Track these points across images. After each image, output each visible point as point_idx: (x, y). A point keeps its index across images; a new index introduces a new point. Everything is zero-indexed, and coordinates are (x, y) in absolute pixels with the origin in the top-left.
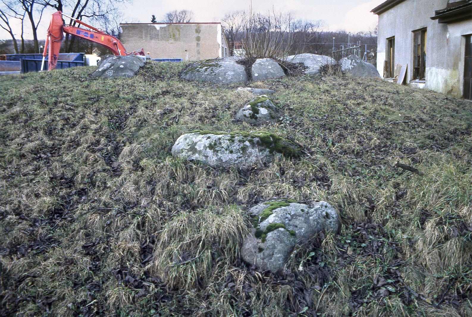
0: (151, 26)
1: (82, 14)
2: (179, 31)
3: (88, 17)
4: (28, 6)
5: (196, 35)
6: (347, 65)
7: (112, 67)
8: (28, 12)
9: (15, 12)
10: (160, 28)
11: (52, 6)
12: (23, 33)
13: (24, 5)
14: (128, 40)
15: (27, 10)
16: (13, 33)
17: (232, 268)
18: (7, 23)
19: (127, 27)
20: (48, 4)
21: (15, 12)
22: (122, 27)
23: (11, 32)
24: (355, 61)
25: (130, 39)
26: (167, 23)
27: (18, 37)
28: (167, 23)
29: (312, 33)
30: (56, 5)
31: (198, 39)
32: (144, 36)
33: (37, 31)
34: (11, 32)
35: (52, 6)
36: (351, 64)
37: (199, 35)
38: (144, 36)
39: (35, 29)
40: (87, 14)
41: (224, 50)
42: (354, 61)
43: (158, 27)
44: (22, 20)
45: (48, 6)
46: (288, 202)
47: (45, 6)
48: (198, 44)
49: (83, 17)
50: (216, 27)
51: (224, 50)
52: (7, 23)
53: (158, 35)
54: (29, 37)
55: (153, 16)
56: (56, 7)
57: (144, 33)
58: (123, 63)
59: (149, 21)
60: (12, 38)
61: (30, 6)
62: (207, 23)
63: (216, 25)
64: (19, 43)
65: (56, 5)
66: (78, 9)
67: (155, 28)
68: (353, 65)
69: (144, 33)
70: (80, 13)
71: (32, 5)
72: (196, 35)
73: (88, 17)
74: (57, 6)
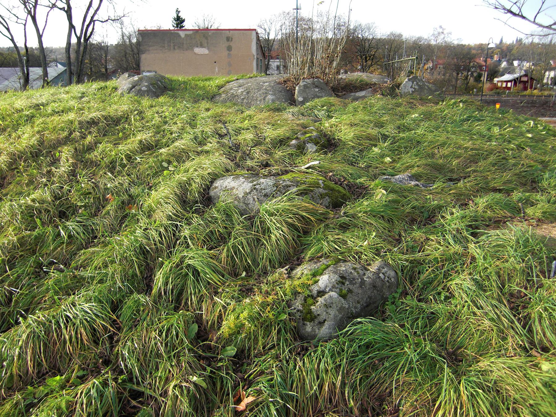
2: (207, 38)
3: (102, 22)
4: (31, 9)
5: (227, 44)
6: (407, 88)
8: (31, 15)
9: (17, 17)
10: (186, 35)
11: (61, 9)
12: (27, 42)
13: (26, 7)
14: (149, 50)
15: (29, 12)
16: (15, 41)
18: (8, 29)
19: (144, 34)
20: (54, 6)
21: (17, 17)
23: (12, 40)
24: (417, 84)
25: (151, 48)
27: (20, 44)
29: (265, 40)
30: (64, 8)
31: (229, 48)
32: (166, 45)
33: (43, 39)
34: (12, 40)
35: (61, 9)
36: (411, 87)
37: (231, 44)
38: (166, 45)
39: (40, 37)
41: (259, 60)
42: (415, 82)
44: (25, 25)
45: (55, 9)
46: (188, 310)
47: (52, 8)
48: (229, 54)
49: (96, 22)
50: (251, 34)
51: (259, 60)
52: (8, 29)
53: (183, 43)
54: (33, 43)
56: (64, 10)
57: (166, 42)
59: (168, 25)
60: (12, 45)
61: (33, 8)
63: (250, 32)
64: (23, 52)
65: (64, 8)
66: (89, 12)
67: (179, 36)
69: (166, 42)
70: (92, 17)
71: (35, 7)
72: (227, 44)
73: (102, 22)
74: (66, 9)
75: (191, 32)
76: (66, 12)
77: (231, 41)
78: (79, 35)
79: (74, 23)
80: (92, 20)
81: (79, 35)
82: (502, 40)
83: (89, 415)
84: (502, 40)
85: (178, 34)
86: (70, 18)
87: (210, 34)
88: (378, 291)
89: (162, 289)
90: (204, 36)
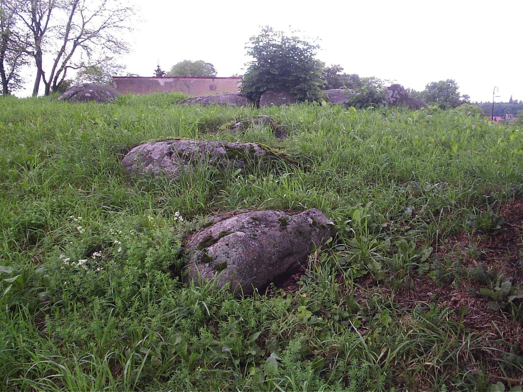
0: (153, 81)
1: (67, 65)
2: (188, 87)
3: (74, 68)
7: (75, 96)
10: (165, 83)
17: (244, 370)
22: (116, 81)
26: (174, 77)
28: (174, 77)
40: (73, 66)
43: (161, 81)
49: (68, 69)
55: (158, 66)
58: (91, 91)
62: (225, 78)
65: (33, 52)
68: (396, 98)
70: (64, 63)
73: (74, 68)
75: (171, 80)
76: (35, 56)
77: (215, 89)
78: (47, 82)
79: (44, 69)
80: (64, 67)
81: (47, 82)
82: (511, 99)
83: (521, 123)
84: (511, 99)
85: (157, 81)
86: (39, 63)
87: (192, 82)
88: (304, 238)
89: (149, 294)
90: (185, 84)
